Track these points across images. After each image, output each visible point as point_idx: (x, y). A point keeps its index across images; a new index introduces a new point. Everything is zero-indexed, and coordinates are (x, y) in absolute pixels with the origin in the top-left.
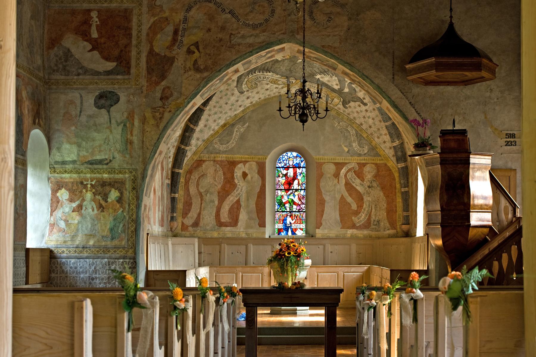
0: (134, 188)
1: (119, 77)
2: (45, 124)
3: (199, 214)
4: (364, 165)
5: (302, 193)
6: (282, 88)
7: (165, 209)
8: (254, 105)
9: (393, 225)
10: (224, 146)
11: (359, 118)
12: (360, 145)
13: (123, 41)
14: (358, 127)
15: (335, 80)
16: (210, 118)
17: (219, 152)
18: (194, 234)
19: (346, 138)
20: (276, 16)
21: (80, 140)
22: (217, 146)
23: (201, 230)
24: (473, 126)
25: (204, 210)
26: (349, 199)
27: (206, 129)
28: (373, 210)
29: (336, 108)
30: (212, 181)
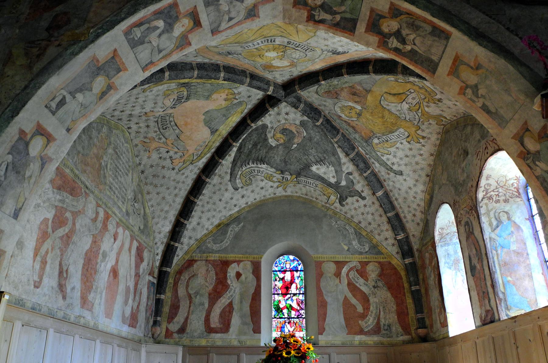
3: (187, 318)
4: (367, 263)
5: (301, 297)
6: (278, 187)
7: (143, 308)
8: (249, 206)
9: (406, 329)
10: (217, 245)
11: (357, 215)
12: (360, 243)
14: (356, 226)
15: (332, 171)
16: (203, 215)
17: (213, 252)
18: (179, 341)
19: (345, 236)
23: (187, 337)
25: (192, 314)
26: (354, 301)
27: (199, 227)
28: (382, 313)
29: (332, 207)
30: (203, 282)
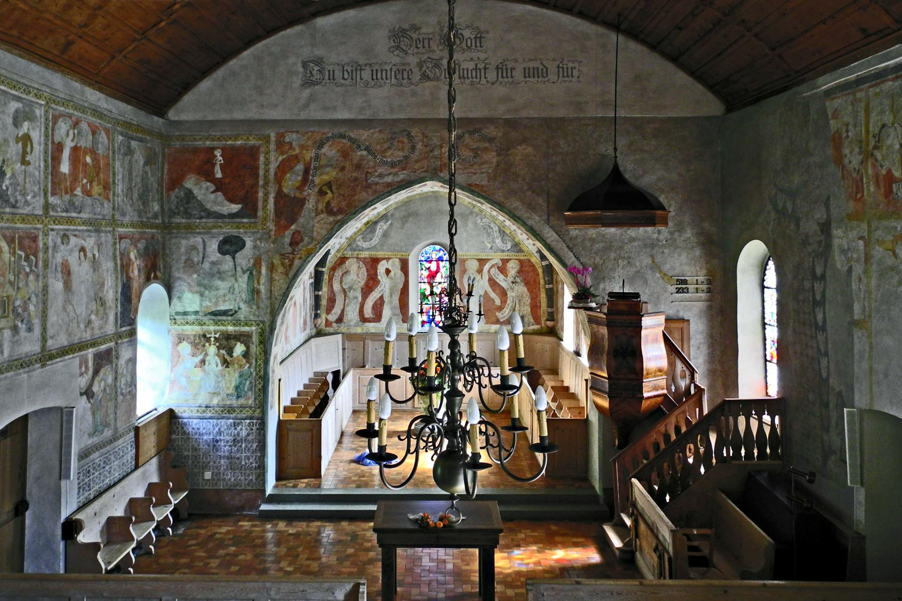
0: (261, 342)
1: (245, 220)
2: (164, 274)
3: (343, 311)
4: (508, 261)
13: (249, 182)
17: (362, 250)
19: (489, 234)
20: (417, 153)
21: (203, 289)
22: (361, 244)
24: (639, 271)
26: (493, 295)
30: (355, 278)
